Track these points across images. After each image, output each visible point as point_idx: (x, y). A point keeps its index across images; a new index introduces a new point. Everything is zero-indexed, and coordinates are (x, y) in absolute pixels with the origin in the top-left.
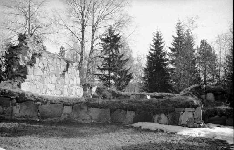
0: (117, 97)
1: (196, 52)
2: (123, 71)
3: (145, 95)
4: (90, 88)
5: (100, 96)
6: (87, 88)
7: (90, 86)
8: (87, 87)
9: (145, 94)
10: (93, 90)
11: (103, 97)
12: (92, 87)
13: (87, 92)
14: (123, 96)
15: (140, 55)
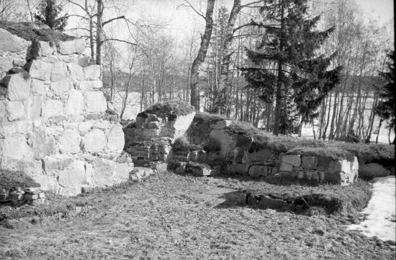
0: (251, 151)
1: (391, 98)
2: (316, 62)
3: (335, 161)
4: (170, 120)
5: (199, 146)
6: (160, 119)
7: (172, 112)
8: (159, 116)
9: (334, 157)
10: (175, 126)
11: (205, 149)
12: (176, 117)
13: (158, 132)
14: (270, 148)
15: (378, 19)
